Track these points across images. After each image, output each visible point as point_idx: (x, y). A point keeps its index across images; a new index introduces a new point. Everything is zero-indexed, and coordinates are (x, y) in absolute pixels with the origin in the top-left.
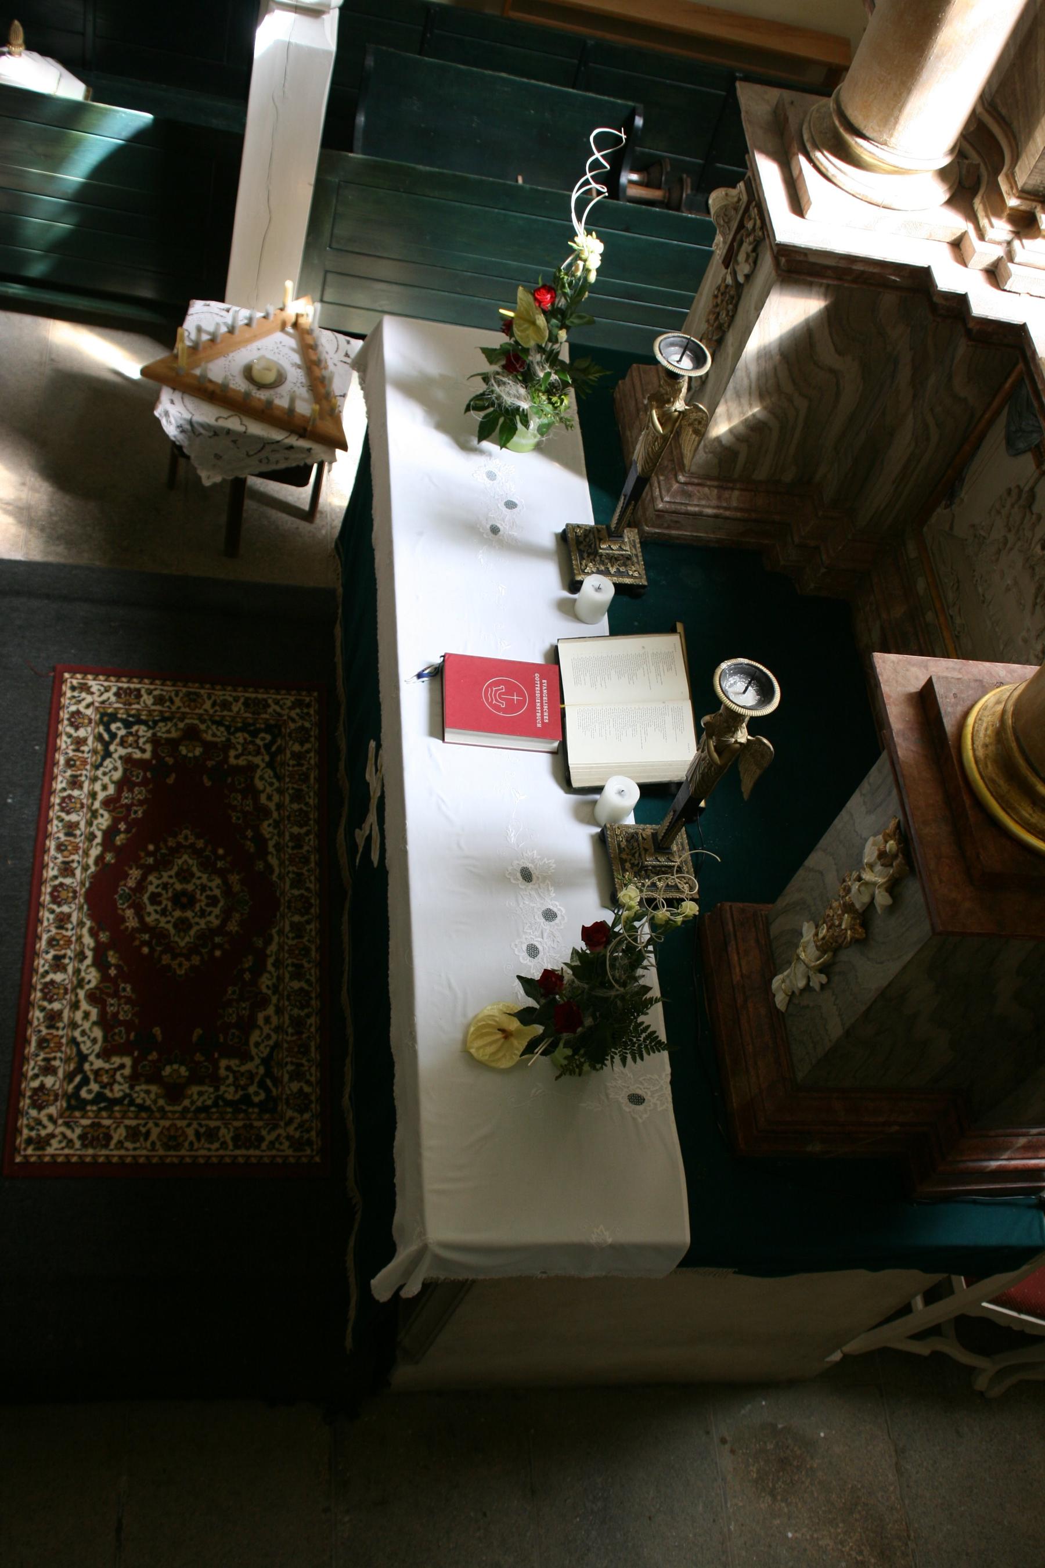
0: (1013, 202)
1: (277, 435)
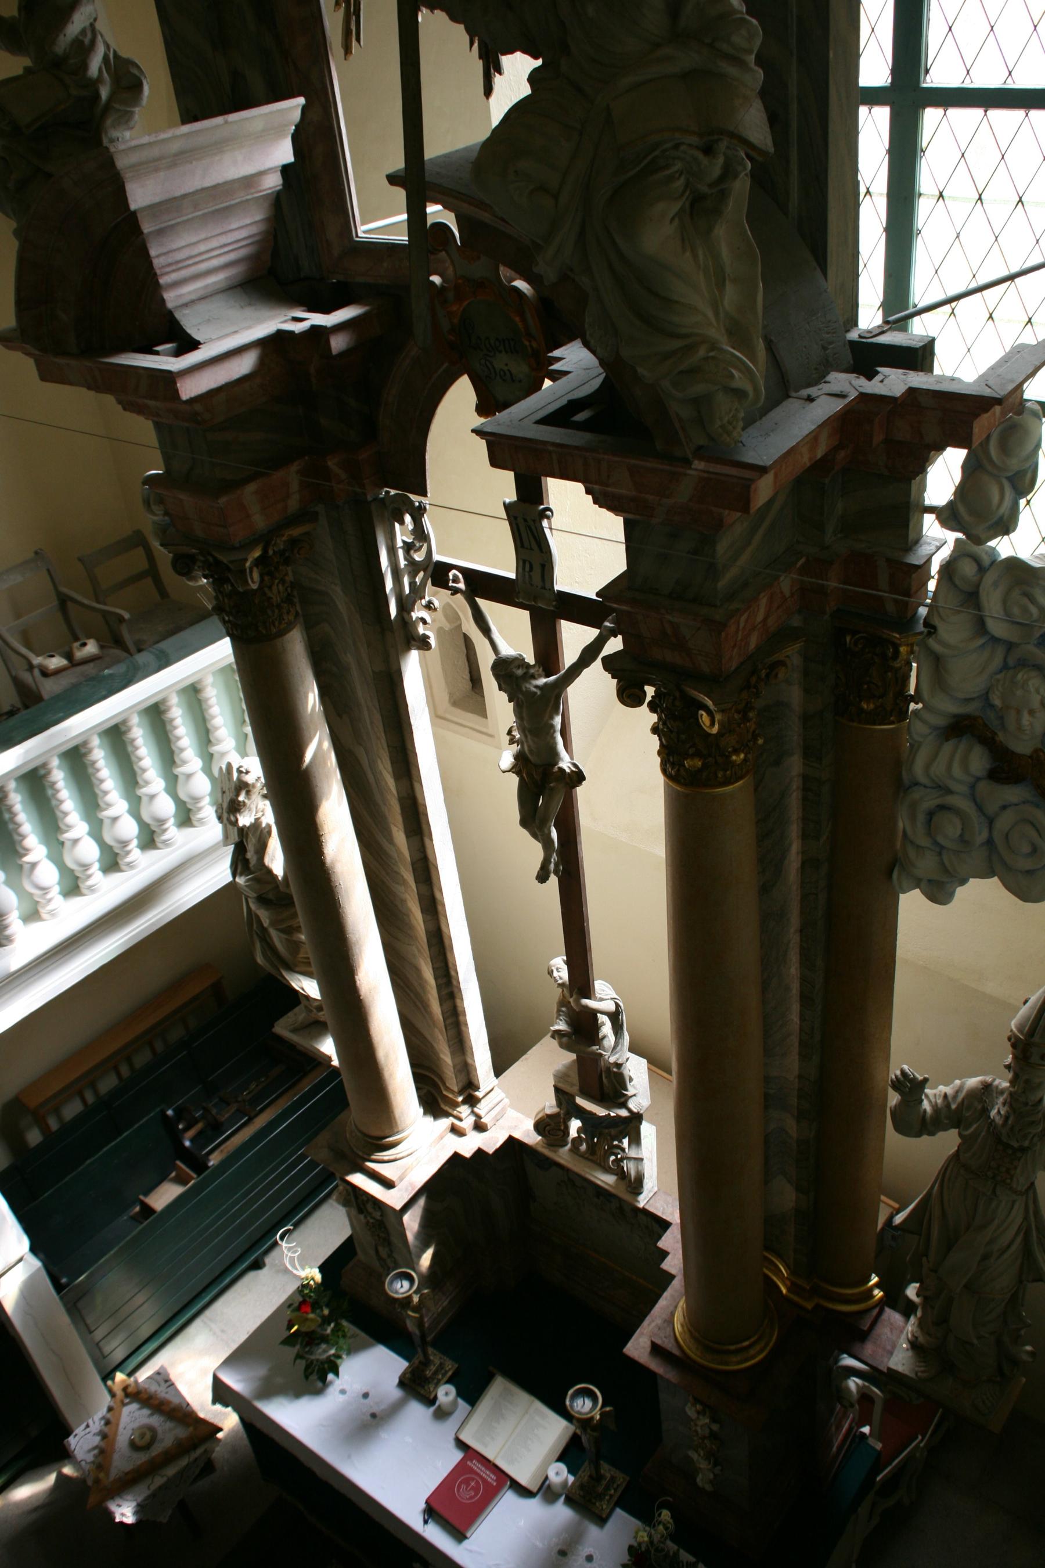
0: (460, 1099)
1: (184, 1462)
